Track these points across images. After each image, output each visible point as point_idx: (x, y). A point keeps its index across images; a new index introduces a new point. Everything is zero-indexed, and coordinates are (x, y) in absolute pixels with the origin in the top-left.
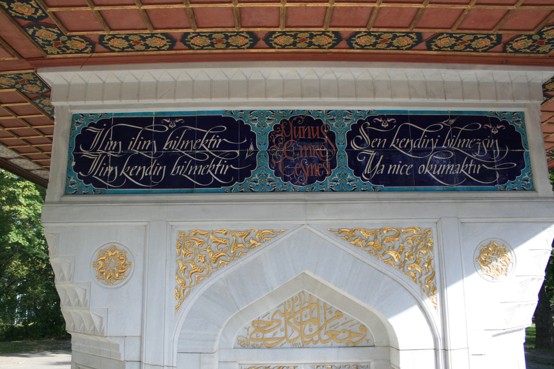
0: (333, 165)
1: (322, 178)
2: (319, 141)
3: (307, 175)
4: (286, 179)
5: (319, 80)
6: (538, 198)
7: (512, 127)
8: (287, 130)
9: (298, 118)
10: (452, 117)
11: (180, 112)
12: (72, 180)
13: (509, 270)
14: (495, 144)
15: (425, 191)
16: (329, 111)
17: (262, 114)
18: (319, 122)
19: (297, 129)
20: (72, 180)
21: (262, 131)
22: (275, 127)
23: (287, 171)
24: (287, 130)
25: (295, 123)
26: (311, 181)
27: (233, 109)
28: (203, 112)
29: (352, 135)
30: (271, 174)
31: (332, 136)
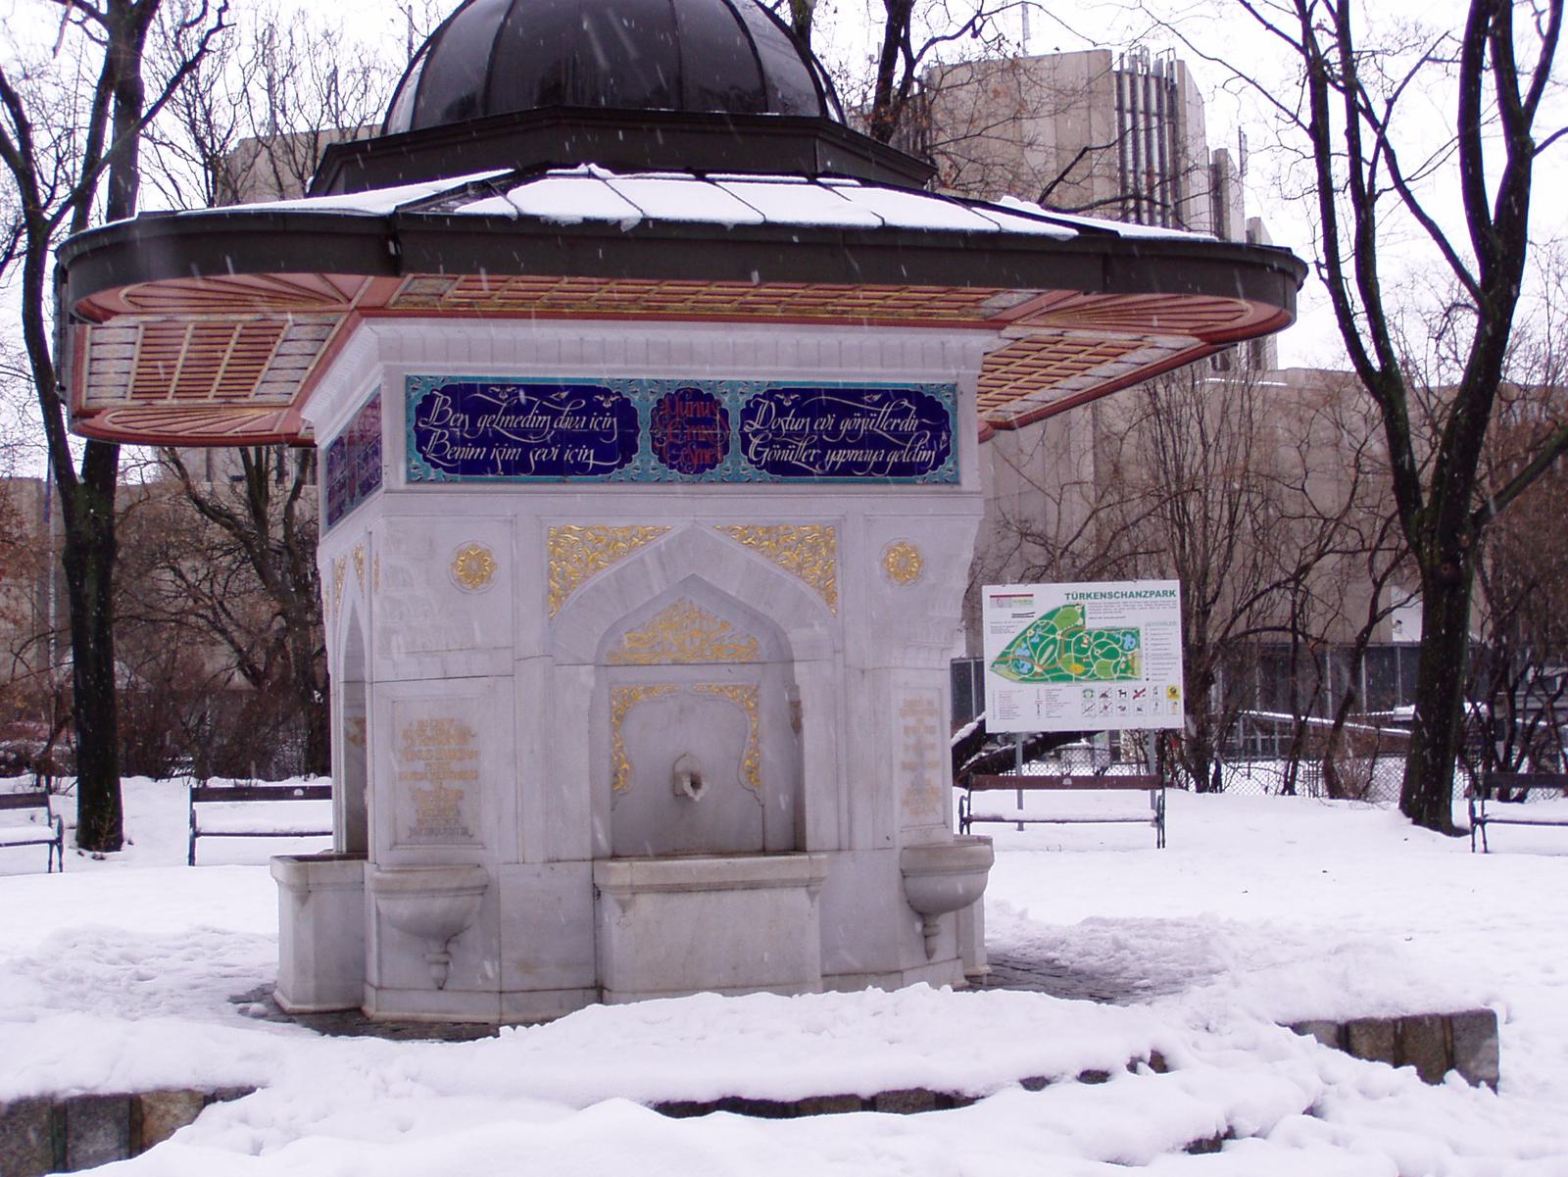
0: (726, 449)
1: (713, 467)
2: (709, 422)
3: (696, 463)
4: (672, 467)
5: (669, 342)
6: (960, 493)
7: (628, 401)
8: (673, 406)
9: (686, 391)
10: (567, 388)
11: (794, 383)
12: (414, 463)
13: (909, 583)
14: (612, 423)
15: (800, 482)
16: (631, 381)
17: (733, 385)
18: (710, 397)
19: (684, 405)
20: (414, 463)
21: (733, 404)
22: (659, 402)
23: (674, 458)
24: (673, 406)
25: (682, 398)
26: (700, 470)
27: (924, 382)
28: (852, 384)
29: (749, 413)
30: (654, 461)
31: (725, 414)
